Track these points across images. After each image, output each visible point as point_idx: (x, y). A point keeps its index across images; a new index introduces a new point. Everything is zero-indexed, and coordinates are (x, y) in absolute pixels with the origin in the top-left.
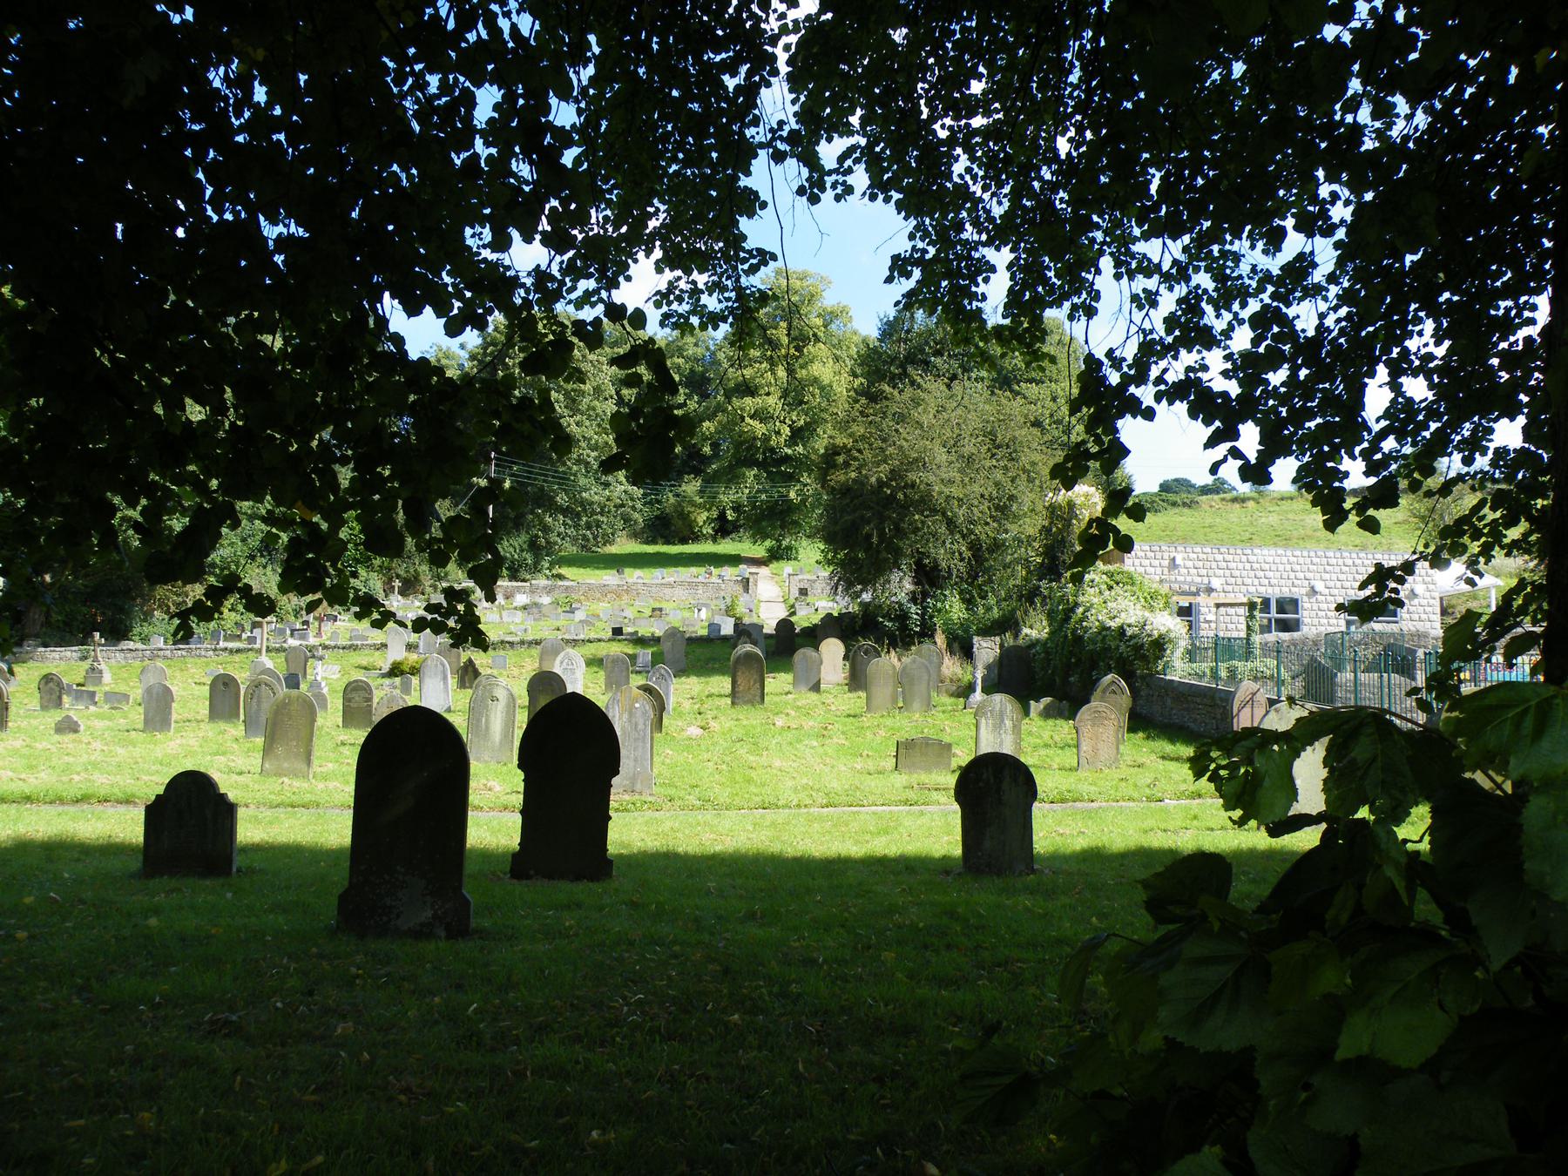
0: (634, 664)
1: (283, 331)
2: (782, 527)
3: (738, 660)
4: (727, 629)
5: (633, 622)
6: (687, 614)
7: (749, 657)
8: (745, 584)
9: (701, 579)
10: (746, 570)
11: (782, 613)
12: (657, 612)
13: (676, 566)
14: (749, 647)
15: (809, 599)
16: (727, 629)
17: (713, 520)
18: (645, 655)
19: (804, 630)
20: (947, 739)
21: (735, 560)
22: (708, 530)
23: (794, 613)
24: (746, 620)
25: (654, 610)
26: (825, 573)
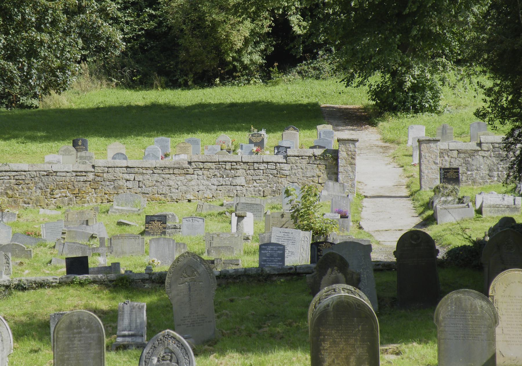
0: (112, 331)
1: (265, 63)
2: (404, 47)
3: (323, 317)
4: (298, 254)
5: (109, 244)
6: (215, 226)
7: (345, 309)
8: (331, 162)
9: (242, 155)
10: (329, 134)
11: (407, 220)
12: (157, 224)
13: (191, 128)
14: (343, 291)
15: (464, 189)
16: (298, 254)
17: (264, 37)
18: (135, 310)
19: (456, 254)
20: (455, 166)
21: (307, 115)
22: (254, 57)
23: (431, 220)
24: (336, 236)
25: (149, 220)
26: (495, 135)
